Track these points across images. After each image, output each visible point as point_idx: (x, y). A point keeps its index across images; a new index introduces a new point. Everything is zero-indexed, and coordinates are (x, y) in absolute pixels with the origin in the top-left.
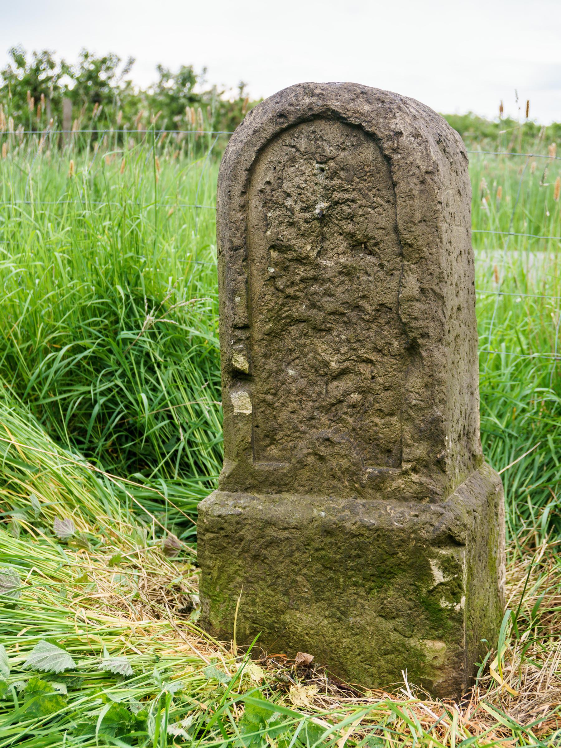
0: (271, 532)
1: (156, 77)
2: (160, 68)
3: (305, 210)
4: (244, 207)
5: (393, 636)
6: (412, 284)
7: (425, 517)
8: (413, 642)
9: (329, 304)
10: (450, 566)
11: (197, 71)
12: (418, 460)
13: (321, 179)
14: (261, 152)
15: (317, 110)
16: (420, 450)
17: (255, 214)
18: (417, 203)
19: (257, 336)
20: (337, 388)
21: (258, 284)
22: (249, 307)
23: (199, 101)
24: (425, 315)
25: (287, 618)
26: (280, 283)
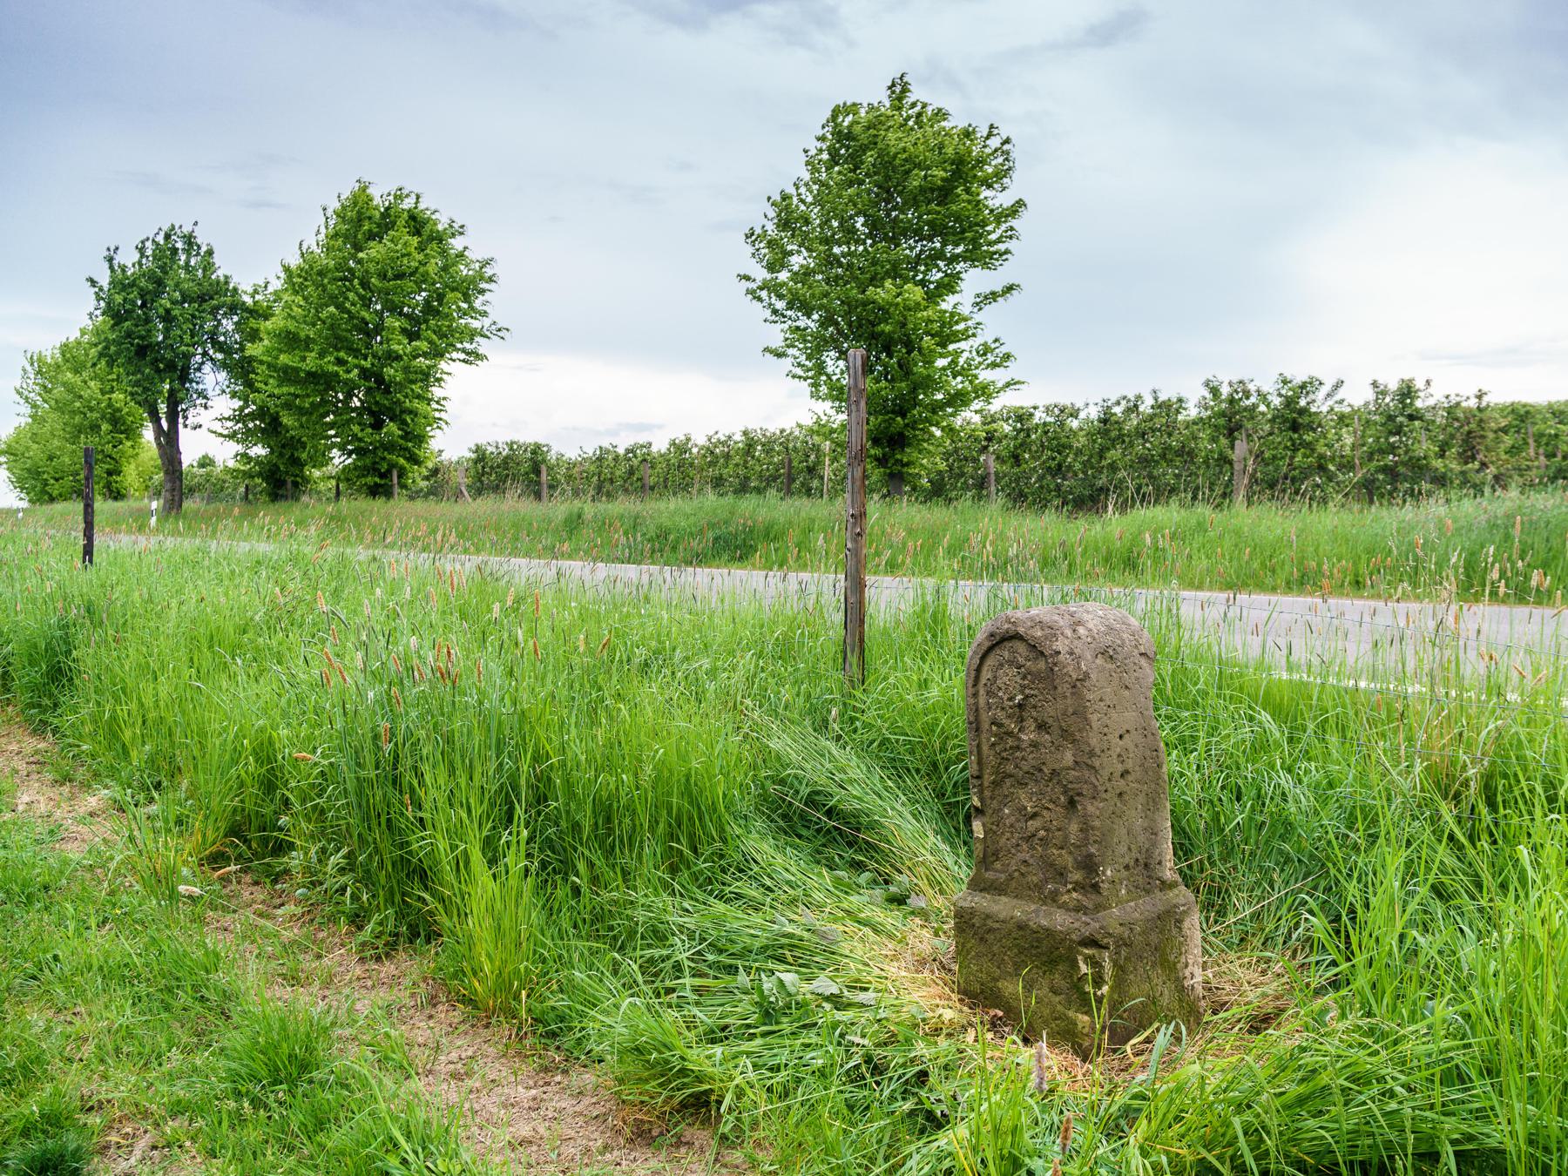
0: (990, 923)
1: (1370, 395)
2: (1375, 384)
3: (1010, 699)
4: (975, 695)
5: (1059, 1007)
6: (1068, 757)
7: (1077, 925)
8: (1071, 1014)
9: (1025, 766)
10: (1095, 964)
11: (1419, 384)
12: (1076, 883)
13: (1018, 679)
14: (983, 658)
15: (1011, 633)
16: (1077, 876)
17: (982, 700)
18: (1069, 701)
19: (986, 784)
20: (1033, 825)
21: (985, 748)
22: (980, 763)
23: (1421, 419)
24: (1078, 780)
25: (1000, 984)
26: (998, 749)
